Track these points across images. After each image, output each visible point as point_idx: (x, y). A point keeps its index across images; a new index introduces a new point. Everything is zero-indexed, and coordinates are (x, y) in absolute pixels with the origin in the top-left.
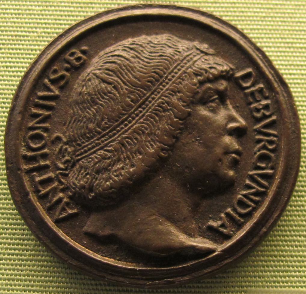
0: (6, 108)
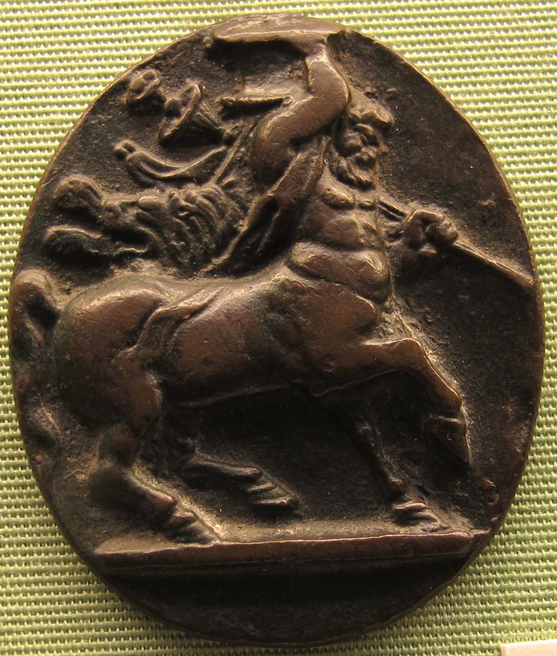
0: (11, 251)
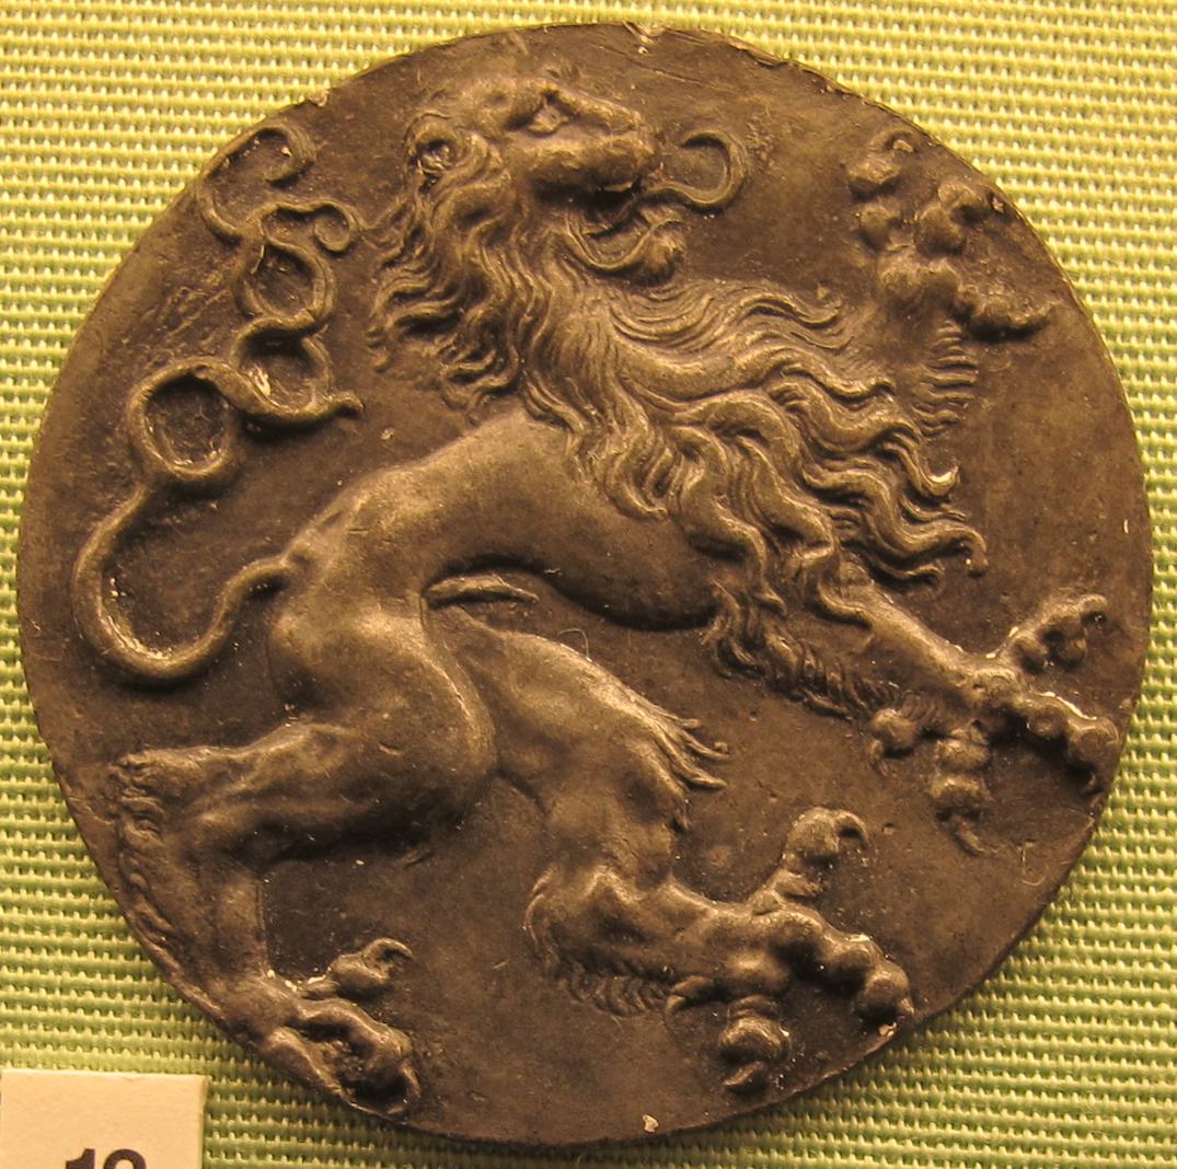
0: (22, 436)
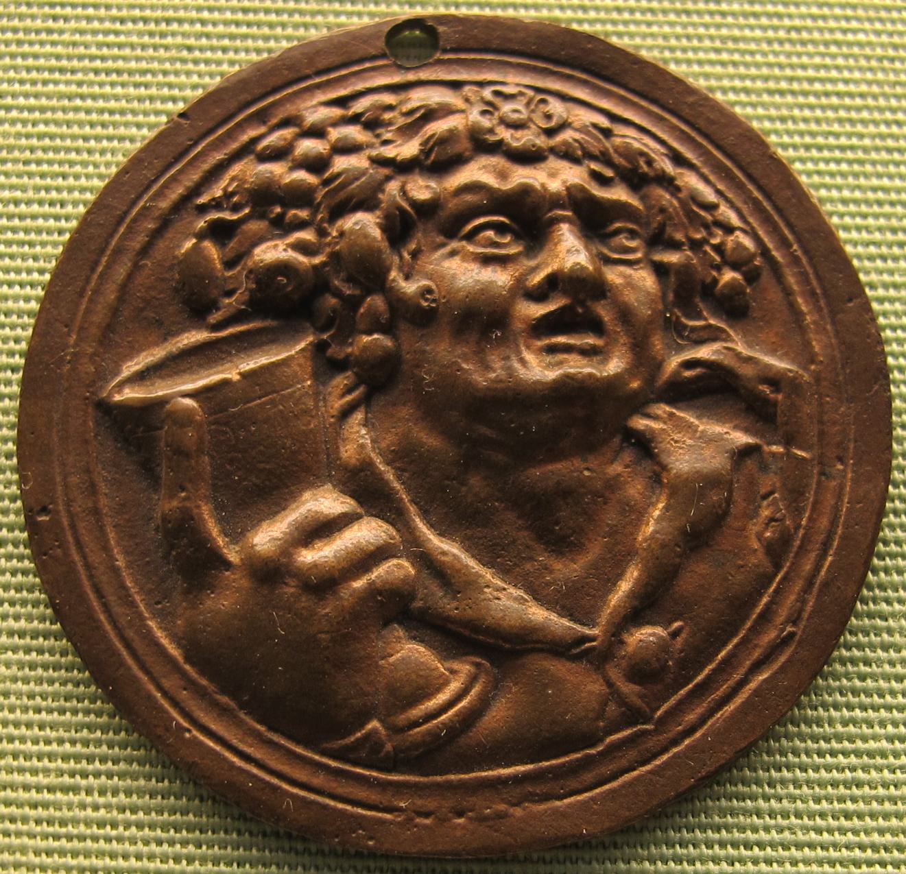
0: (17, 340)
